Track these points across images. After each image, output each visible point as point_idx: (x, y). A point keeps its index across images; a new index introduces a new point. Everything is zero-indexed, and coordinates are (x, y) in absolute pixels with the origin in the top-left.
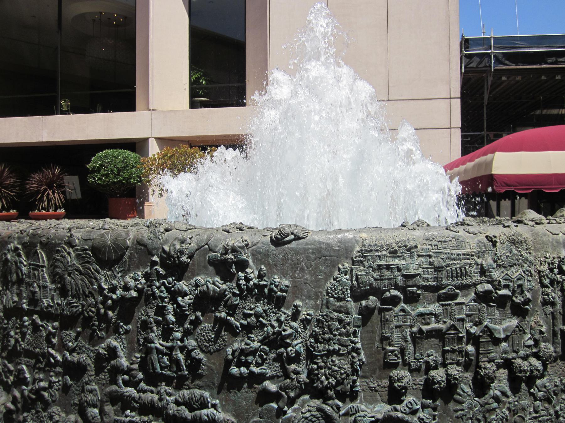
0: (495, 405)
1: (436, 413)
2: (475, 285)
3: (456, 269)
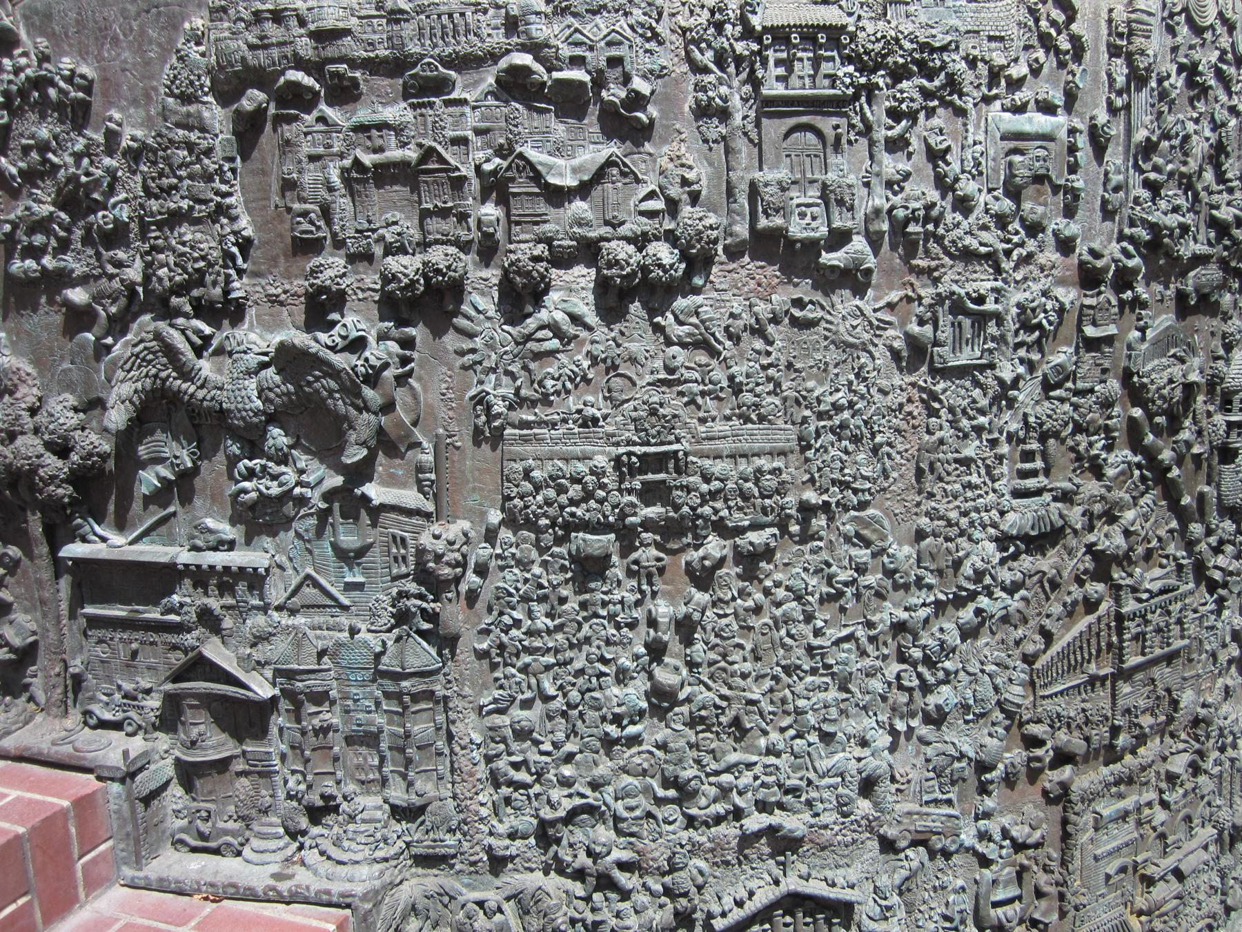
0: (555, 344)
2: (494, 57)
3: (439, 16)
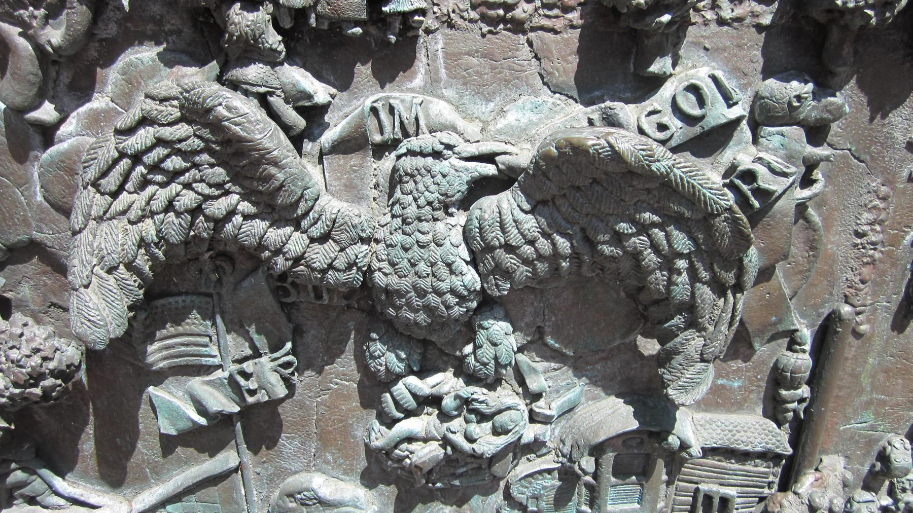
1: (822, 151)
